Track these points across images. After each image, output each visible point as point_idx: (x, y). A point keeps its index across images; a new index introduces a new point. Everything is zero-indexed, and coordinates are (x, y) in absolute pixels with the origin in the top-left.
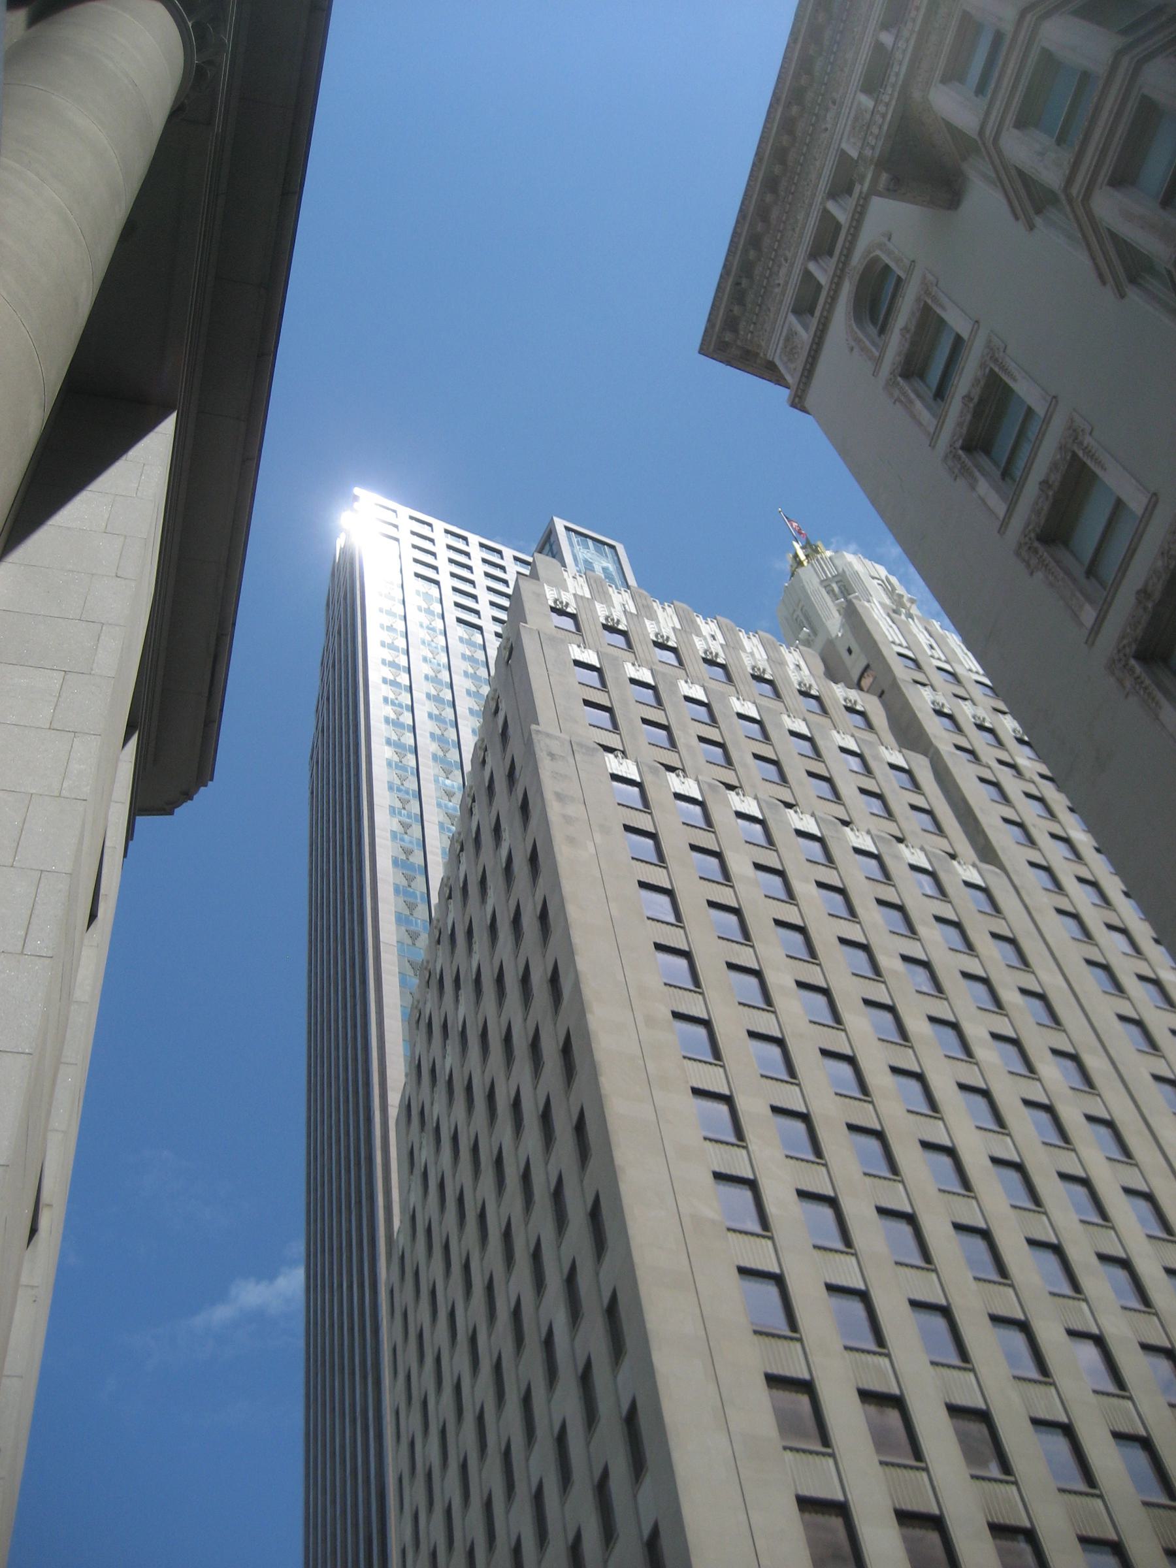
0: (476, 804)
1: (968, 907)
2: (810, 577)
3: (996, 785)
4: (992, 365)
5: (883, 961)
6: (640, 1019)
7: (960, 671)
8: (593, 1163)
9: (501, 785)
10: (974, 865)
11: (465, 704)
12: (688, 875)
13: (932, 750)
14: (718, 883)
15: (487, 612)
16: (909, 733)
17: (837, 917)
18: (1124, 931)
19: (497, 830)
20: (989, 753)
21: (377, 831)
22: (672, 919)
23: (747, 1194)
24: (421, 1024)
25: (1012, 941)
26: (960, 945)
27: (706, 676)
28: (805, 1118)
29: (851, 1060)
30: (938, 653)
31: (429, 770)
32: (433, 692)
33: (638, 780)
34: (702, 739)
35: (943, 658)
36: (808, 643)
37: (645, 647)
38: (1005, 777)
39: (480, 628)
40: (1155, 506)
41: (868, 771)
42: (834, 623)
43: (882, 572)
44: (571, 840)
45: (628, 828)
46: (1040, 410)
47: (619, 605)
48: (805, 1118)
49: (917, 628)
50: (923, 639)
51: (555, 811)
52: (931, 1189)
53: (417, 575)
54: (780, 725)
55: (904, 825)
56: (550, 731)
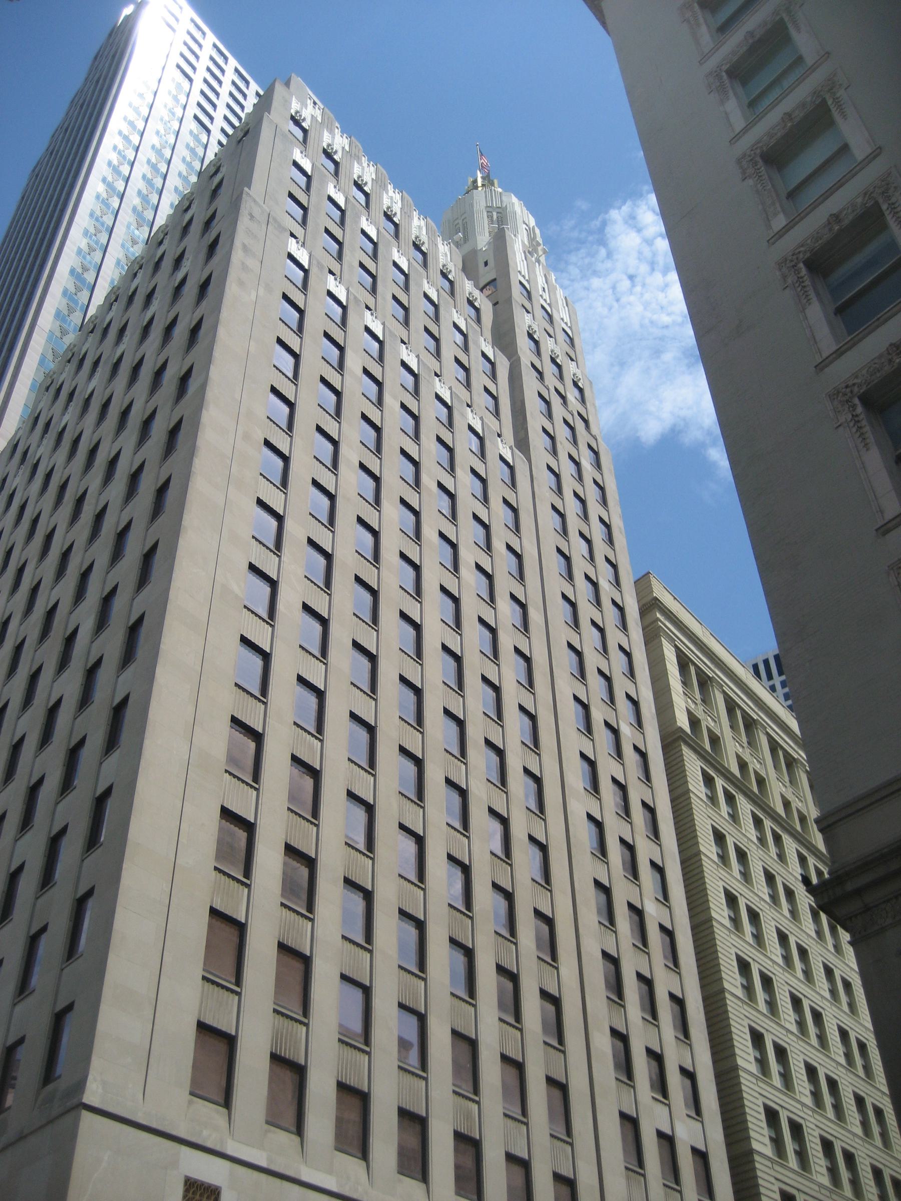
0: (142, 271)
1: (496, 474)
2: (480, 198)
3: (548, 403)
4: (784, 15)
5: (425, 478)
6: (240, 432)
7: (556, 316)
8: (162, 519)
9: (167, 264)
10: (511, 448)
11: (173, 181)
12: (315, 351)
13: (514, 358)
14: (333, 367)
15: (219, 122)
16: (503, 337)
17: (406, 433)
18: (589, 542)
19: (150, 297)
20: (551, 380)
21: (65, 248)
22: (290, 375)
23: (267, 590)
24: (51, 388)
25: (515, 510)
26: (479, 494)
27: (382, 225)
28: (328, 557)
29: (375, 534)
30: (546, 296)
31: (126, 217)
32: (154, 160)
33: (307, 267)
34: (362, 265)
35: (548, 301)
36: (458, 245)
37: (347, 181)
38: (556, 401)
39: (208, 131)
40: (875, 157)
41: (466, 348)
42: (483, 240)
43: (532, 222)
44: (241, 283)
45: (285, 297)
46: (809, 60)
47: (339, 142)
48: (328, 557)
49: (539, 272)
50: (541, 281)
51: (237, 255)
52: (396, 646)
53: (178, 66)
54: (421, 285)
55: (475, 397)
56: (257, 199)
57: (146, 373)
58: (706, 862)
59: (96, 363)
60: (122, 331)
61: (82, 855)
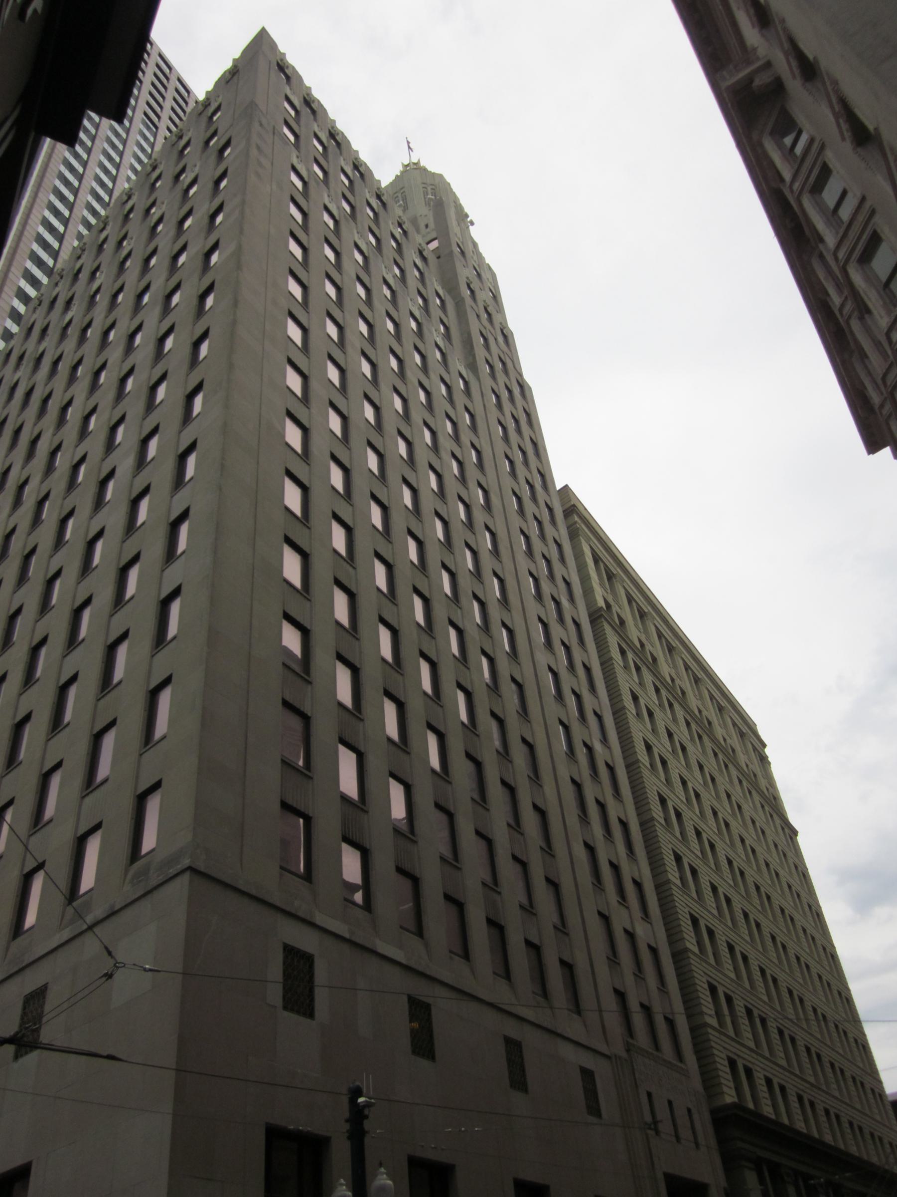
0: (63, 281)
19: (69, 303)
57: (64, 368)
58: (629, 716)
59: (21, 358)
60: (44, 331)
61: (48, 735)
